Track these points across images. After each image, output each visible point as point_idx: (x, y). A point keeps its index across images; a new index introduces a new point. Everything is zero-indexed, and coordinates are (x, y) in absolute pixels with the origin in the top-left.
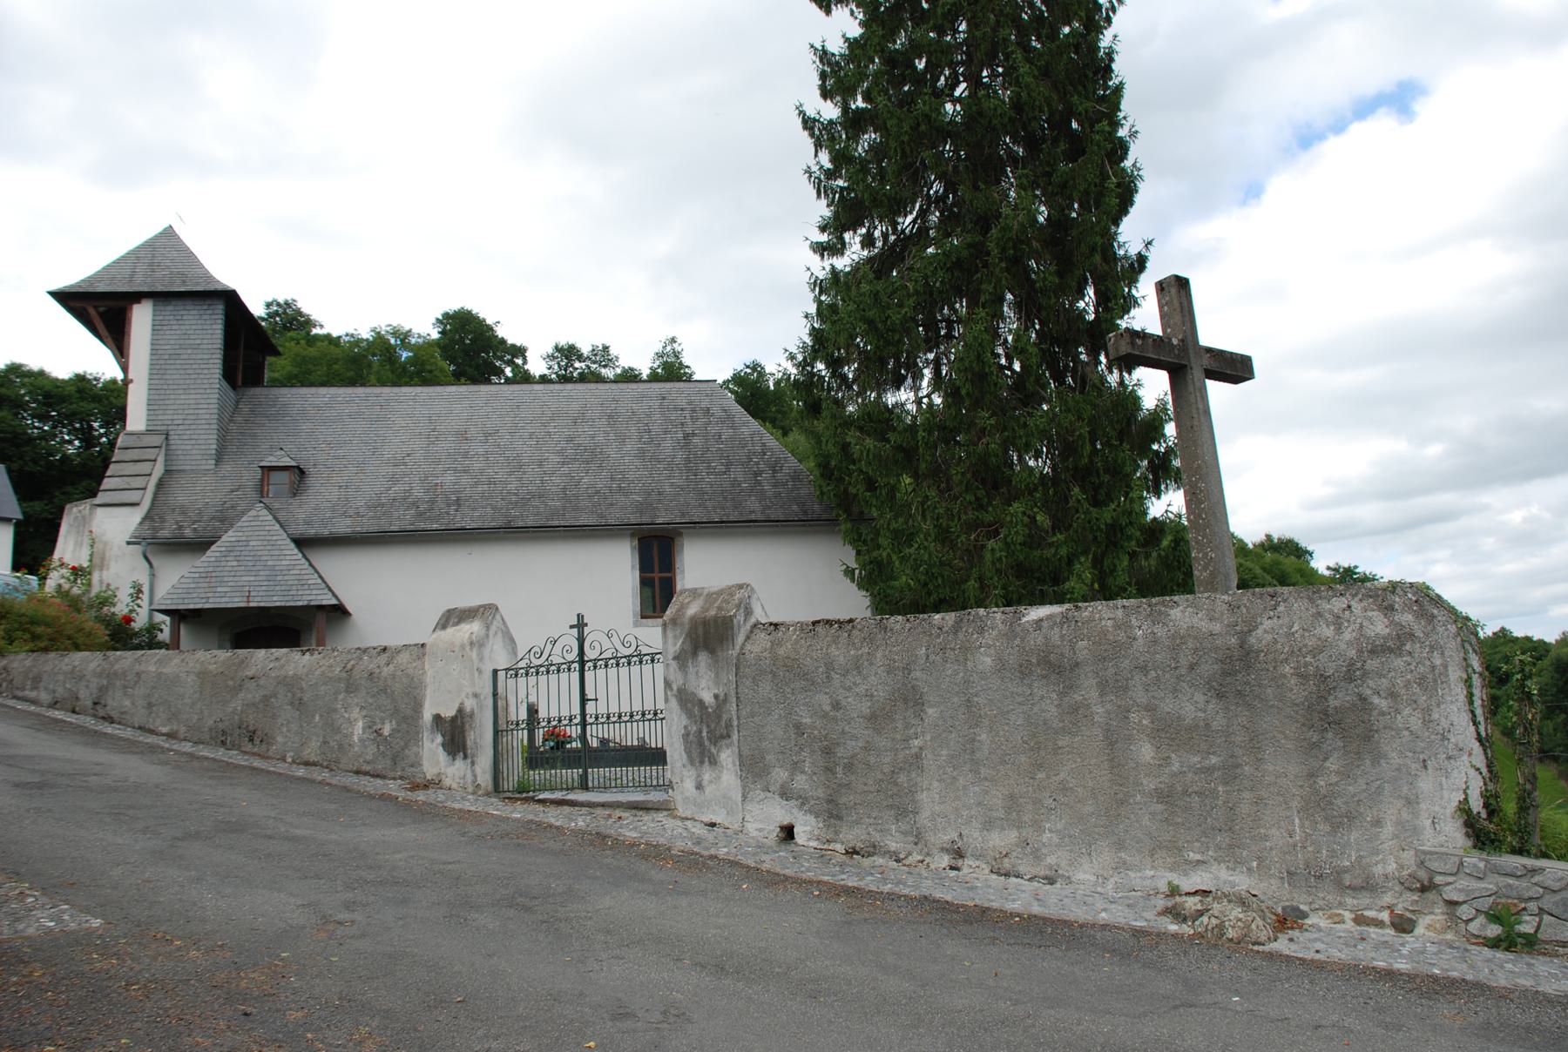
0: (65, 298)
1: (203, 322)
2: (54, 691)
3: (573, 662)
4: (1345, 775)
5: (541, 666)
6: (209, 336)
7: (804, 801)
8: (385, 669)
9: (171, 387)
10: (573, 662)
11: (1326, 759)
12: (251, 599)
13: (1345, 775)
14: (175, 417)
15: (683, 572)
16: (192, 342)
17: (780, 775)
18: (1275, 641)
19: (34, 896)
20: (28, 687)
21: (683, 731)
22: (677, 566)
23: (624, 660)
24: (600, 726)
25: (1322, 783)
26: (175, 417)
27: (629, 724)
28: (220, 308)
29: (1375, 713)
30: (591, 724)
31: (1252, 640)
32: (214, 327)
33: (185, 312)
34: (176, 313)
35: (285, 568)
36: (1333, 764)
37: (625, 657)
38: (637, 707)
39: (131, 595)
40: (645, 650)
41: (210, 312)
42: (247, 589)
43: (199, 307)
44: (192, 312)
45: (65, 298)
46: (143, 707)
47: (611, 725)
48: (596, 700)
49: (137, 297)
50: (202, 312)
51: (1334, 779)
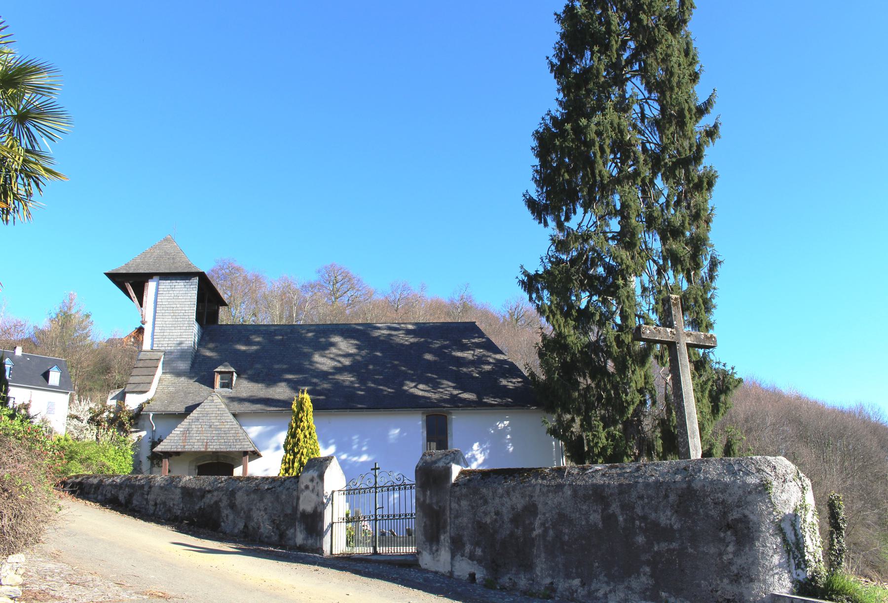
0: (107, 274)
1: (186, 289)
2: (105, 495)
3: (372, 488)
4: (736, 554)
5: (356, 489)
6: (189, 298)
7: (480, 562)
8: (279, 489)
9: (179, 320)
10: (372, 488)
11: (727, 546)
12: (208, 447)
13: (736, 554)
14: (170, 342)
15: (452, 435)
16: (180, 300)
17: (468, 548)
18: (704, 486)
19: (777, 573)
20: (92, 492)
21: (423, 525)
22: (448, 432)
23: (397, 487)
24: (384, 521)
25: (725, 558)
26: (170, 342)
27: (398, 520)
28: (196, 280)
29: (751, 523)
30: (380, 520)
31: (693, 485)
32: (192, 292)
33: (177, 284)
34: (171, 284)
35: (227, 429)
36: (731, 549)
37: (397, 485)
38: (403, 512)
39: (714, 299)
40: (407, 482)
41: (190, 284)
42: (206, 441)
43: (184, 281)
44: (180, 284)
45: (107, 274)
46: (152, 505)
47: (401, 520)
48: (383, 507)
49: (149, 276)
50: (186, 284)
51: (731, 556)
